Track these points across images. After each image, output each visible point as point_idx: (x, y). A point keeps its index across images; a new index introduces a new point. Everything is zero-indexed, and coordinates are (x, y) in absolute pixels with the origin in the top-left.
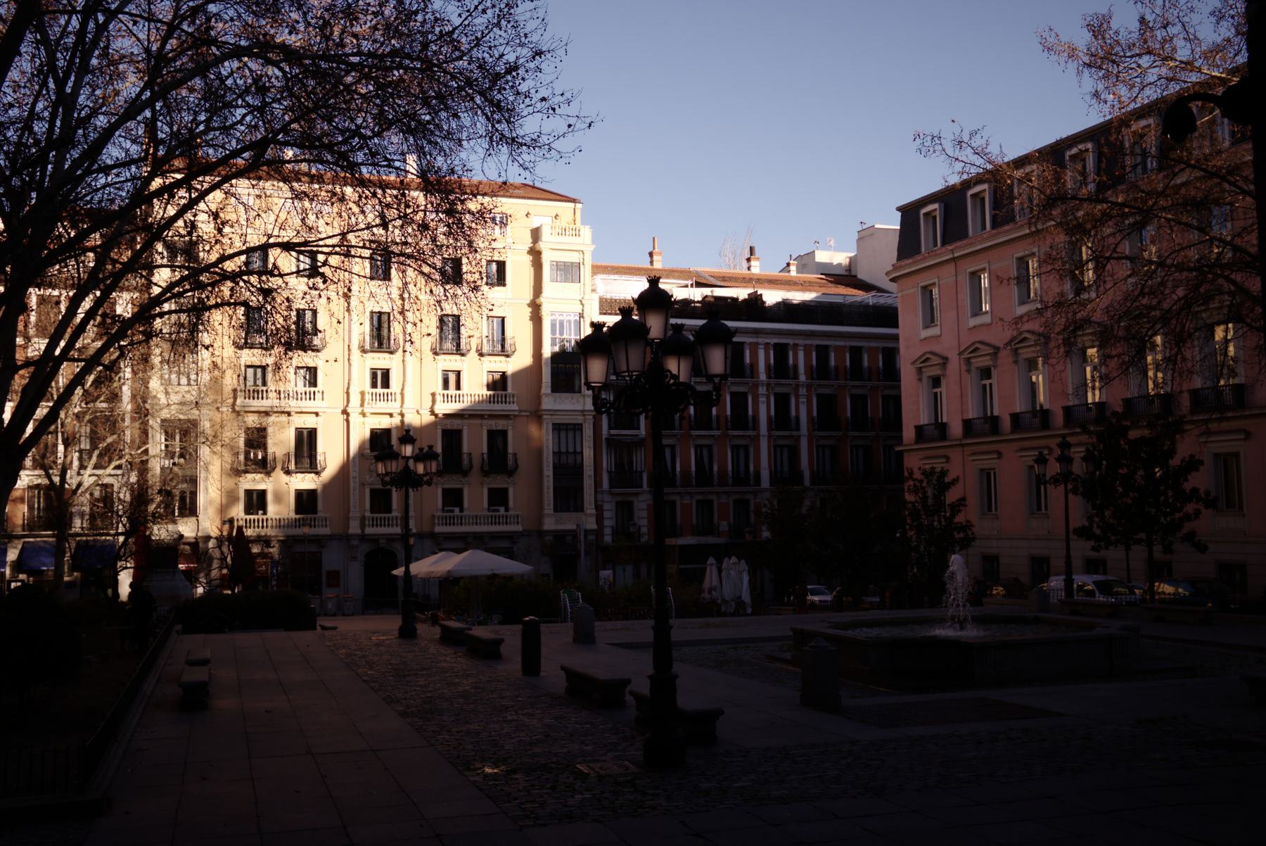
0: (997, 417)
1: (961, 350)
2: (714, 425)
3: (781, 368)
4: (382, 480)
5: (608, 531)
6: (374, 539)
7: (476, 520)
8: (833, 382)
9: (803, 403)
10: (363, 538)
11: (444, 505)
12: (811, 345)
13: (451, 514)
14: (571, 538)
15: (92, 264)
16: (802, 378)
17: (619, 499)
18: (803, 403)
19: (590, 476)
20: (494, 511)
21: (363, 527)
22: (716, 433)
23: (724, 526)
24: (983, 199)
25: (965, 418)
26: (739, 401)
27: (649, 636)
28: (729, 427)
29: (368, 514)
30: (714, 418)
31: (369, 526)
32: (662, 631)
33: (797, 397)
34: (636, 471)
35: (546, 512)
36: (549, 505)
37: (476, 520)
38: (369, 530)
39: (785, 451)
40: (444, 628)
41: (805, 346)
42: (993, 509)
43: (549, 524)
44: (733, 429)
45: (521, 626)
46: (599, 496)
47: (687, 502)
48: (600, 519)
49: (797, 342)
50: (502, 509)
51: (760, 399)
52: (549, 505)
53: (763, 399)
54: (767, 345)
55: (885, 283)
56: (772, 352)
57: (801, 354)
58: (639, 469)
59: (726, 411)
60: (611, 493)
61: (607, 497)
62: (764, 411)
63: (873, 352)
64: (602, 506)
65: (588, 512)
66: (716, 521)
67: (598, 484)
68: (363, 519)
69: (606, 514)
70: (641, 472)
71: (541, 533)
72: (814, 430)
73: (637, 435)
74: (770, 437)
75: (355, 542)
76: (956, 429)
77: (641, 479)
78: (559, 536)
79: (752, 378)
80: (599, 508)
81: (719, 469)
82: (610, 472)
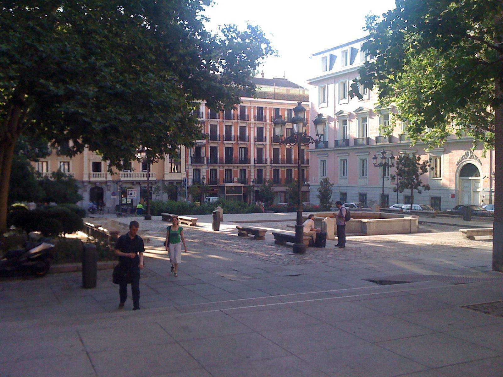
0: (348, 140)
1: (336, 113)
2: (233, 139)
3: (260, 117)
4: (375, 165)
5: (190, 180)
6: (95, 183)
7: (137, 176)
8: (218, 120)
9: (252, 130)
10: (90, 182)
11: (142, 170)
12: (272, 108)
13: (127, 173)
14: (176, 183)
15: (494, 113)
16: (268, 121)
17: (195, 168)
18: (268, 131)
19: (184, 158)
20: (125, 172)
21: (89, 177)
22: (235, 142)
23: (236, 179)
24: (347, 53)
25: (336, 140)
26: (243, 129)
27: (295, 218)
28: (224, 139)
29: (91, 172)
30: (218, 136)
31: (92, 177)
32: (299, 216)
33: (266, 129)
34: (202, 157)
35: (166, 172)
36: (167, 170)
37: (137, 176)
38: (92, 179)
39: (243, 150)
40: (163, 216)
41: (270, 108)
42: (325, 175)
43: (168, 177)
44: (274, 142)
45: (161, 217)
46: (187, 166)
47: (283, 170)
48: (187, 175)
49: (266, 106)
50: (129, 171)
51: (251, 129)
52: (167, 170)
53: (252, 129)
54: (254, 107)
55: (305, 85)
56: (256, 110)
57: (268, 111)
58: (203, 156)
59: (237, 134)
60: (191, 165)
61: (190, 167)
62: (252, 133)
63: (270, 109)
64: (188, 170)
65: (183, 173)
66: (233, 177)
67: (186, 161)
68: (89, 174)
69: (190, 174)
70: (204, 157)
71: (163, 181)
72: (272, 142)
73: (202, 142)
74: (255, 144)
75: (86, 184)
76: (331, 144)
77: (204, 160)
78: (171, 182)
79: (248, 120)
80: (187, 171)
81: (294, 158)
82: (191, 157)
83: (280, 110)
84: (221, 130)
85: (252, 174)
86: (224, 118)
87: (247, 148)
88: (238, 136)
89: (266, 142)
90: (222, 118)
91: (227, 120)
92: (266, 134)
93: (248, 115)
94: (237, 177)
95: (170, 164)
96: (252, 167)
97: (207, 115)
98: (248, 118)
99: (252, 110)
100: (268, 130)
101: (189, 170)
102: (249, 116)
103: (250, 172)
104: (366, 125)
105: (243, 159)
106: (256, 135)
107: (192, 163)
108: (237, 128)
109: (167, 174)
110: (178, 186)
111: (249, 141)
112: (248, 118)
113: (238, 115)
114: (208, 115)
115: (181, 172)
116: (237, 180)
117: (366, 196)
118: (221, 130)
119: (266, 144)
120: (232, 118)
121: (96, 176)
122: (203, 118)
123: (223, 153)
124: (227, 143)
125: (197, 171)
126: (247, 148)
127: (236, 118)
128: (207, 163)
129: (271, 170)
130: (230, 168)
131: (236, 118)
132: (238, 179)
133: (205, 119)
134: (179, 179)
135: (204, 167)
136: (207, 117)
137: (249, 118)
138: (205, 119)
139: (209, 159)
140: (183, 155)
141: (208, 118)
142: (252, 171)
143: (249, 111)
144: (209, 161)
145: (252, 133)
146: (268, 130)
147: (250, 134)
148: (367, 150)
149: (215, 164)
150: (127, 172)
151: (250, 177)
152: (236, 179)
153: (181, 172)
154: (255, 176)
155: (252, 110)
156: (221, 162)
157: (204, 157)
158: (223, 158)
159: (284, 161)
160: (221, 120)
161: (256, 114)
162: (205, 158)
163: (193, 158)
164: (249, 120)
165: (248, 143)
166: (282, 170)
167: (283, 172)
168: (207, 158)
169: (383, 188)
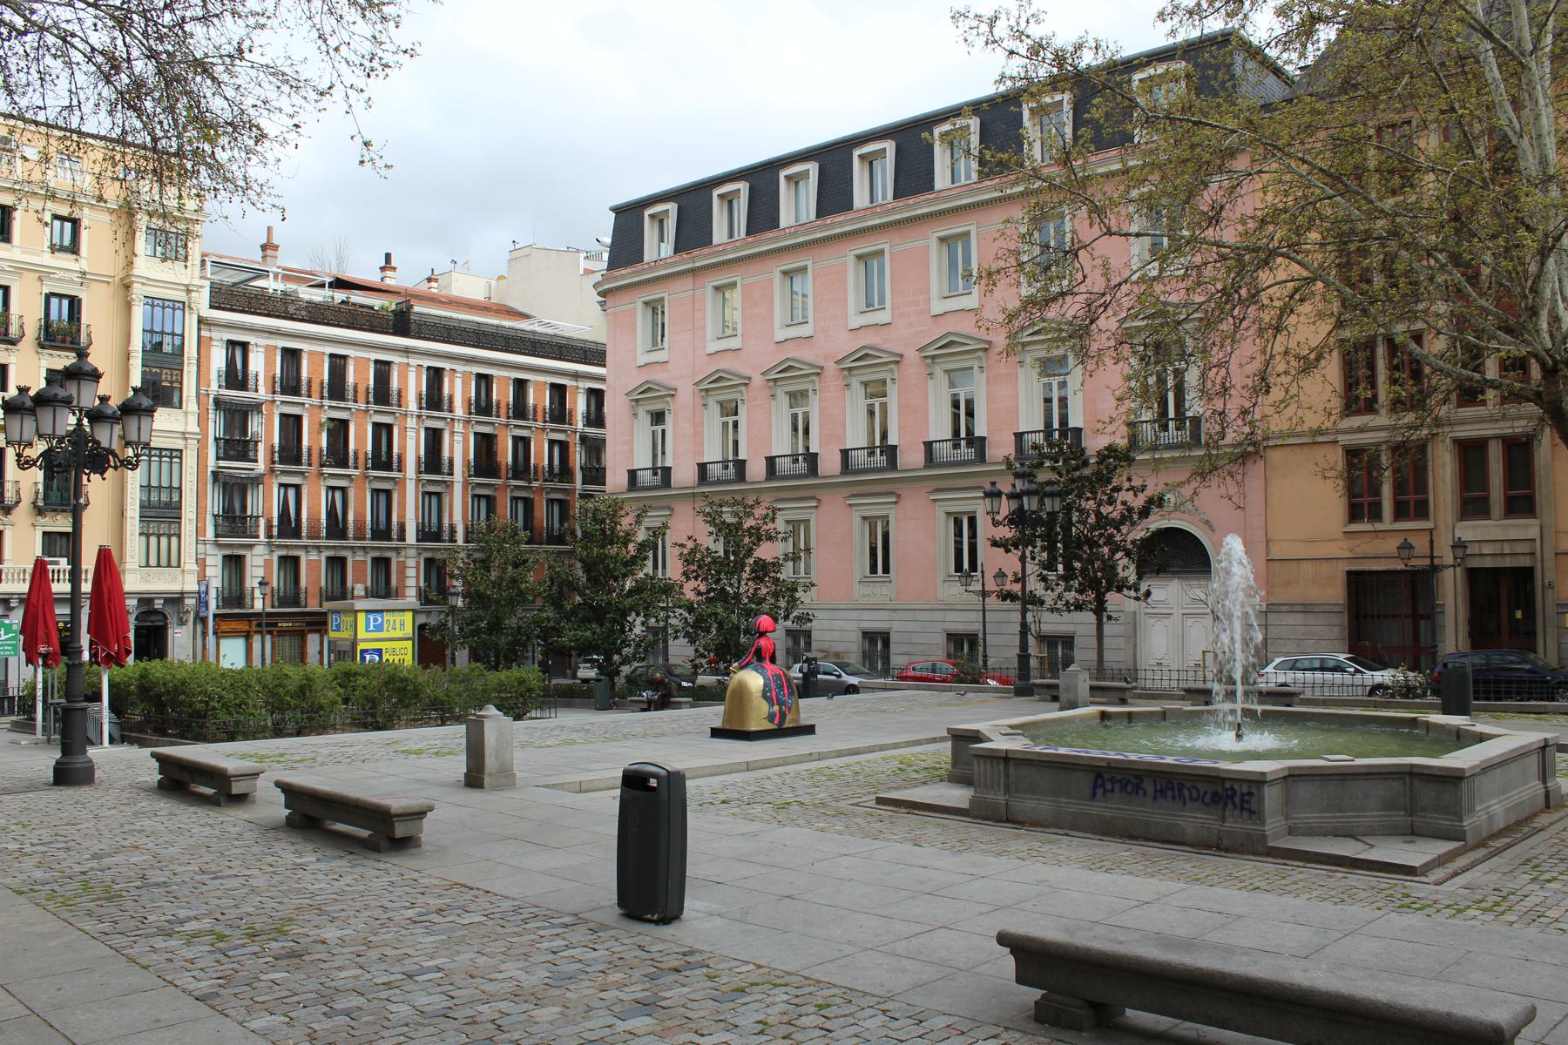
8: (350, 404)
16: (459, 411)
22: (356, 472)
48: (202, 578)
49: (454, 367)
56: (424, 377)
57: (458, 383)
61: (210, 549)
62: (411, 445)
65: (187, 567)
66: (349, 584)
67: (200, 531)
69: (210, 572)
70: (258, 517)
74: (418, 480)
80: (201, 563)
83: (495, 381)
84: (361, 438)
85: (411, 572)
86: (326, 395)
87: (495, 498)
88: (321, 450)
89: (452, 474)
90: (318, 395)
91: (334, 403)
92: (403, 447)
93: (399, 392)
94: (365, 582)
95: (143, 539)
96: (413, 552)
97: (466, 404)
98: (399, 401)
99: (412, 377)
100: (458, 438)
101: (208, 558)
102: (403, 394)
103: (402, 567)
104: (663, 431)
105: (434, 529)
106: (422, 452)
107: (217, 536)
108: (366, 430)
109: (133, 571)
110: (169, 611)
111: (400, 471)
112: (399, 401)
113: (322, 383)
114: (274, 382)
115: (179, 566)
116: (363, 593)
117: (810, 637)
118: (361, 438)
119: (405, 479)
120: (350, 395)
121: (61, 577)
122: (256, 391)
123: (320, 505)
124: (331, 475)
125: (235, 563)
126: (495, 498)
127: (361, 397)
128: (269, 536)
129: (267, 557)
130: (342, 553)
131: (361, 397)
132: (366, 589)
133: (263, 393)
134: (175, 587)
135: (259, 550)
136: (270, 388)
137: (403, 399)
138: (263, 393)
139: (275, 523)
140: (189, 509)
141: (274, 393)
142: (411, 563)
143: (403, 377)
144: (275, 531)
145: (411, 445)
146: (458, 438)
147: (405, 446)
148: (664, 503)
149: (385, 544)
150: (57, 563)
151: (404, 581)
152: (359, 590)
153: (179, 566)
154: (418, 582)
155: (412, 377)
156: (360, 536)
157: (258, 517)
158: (319, 520)
159: (319, 531)
160: (315, 400)
161: (424, 389)
162: (262, 522)
163: (220, 520)
164: (403, 403)
165: (447, 478)
166: (358, 558)
167: (359, 565)
168: (269, 526)
169: (984, 610)
